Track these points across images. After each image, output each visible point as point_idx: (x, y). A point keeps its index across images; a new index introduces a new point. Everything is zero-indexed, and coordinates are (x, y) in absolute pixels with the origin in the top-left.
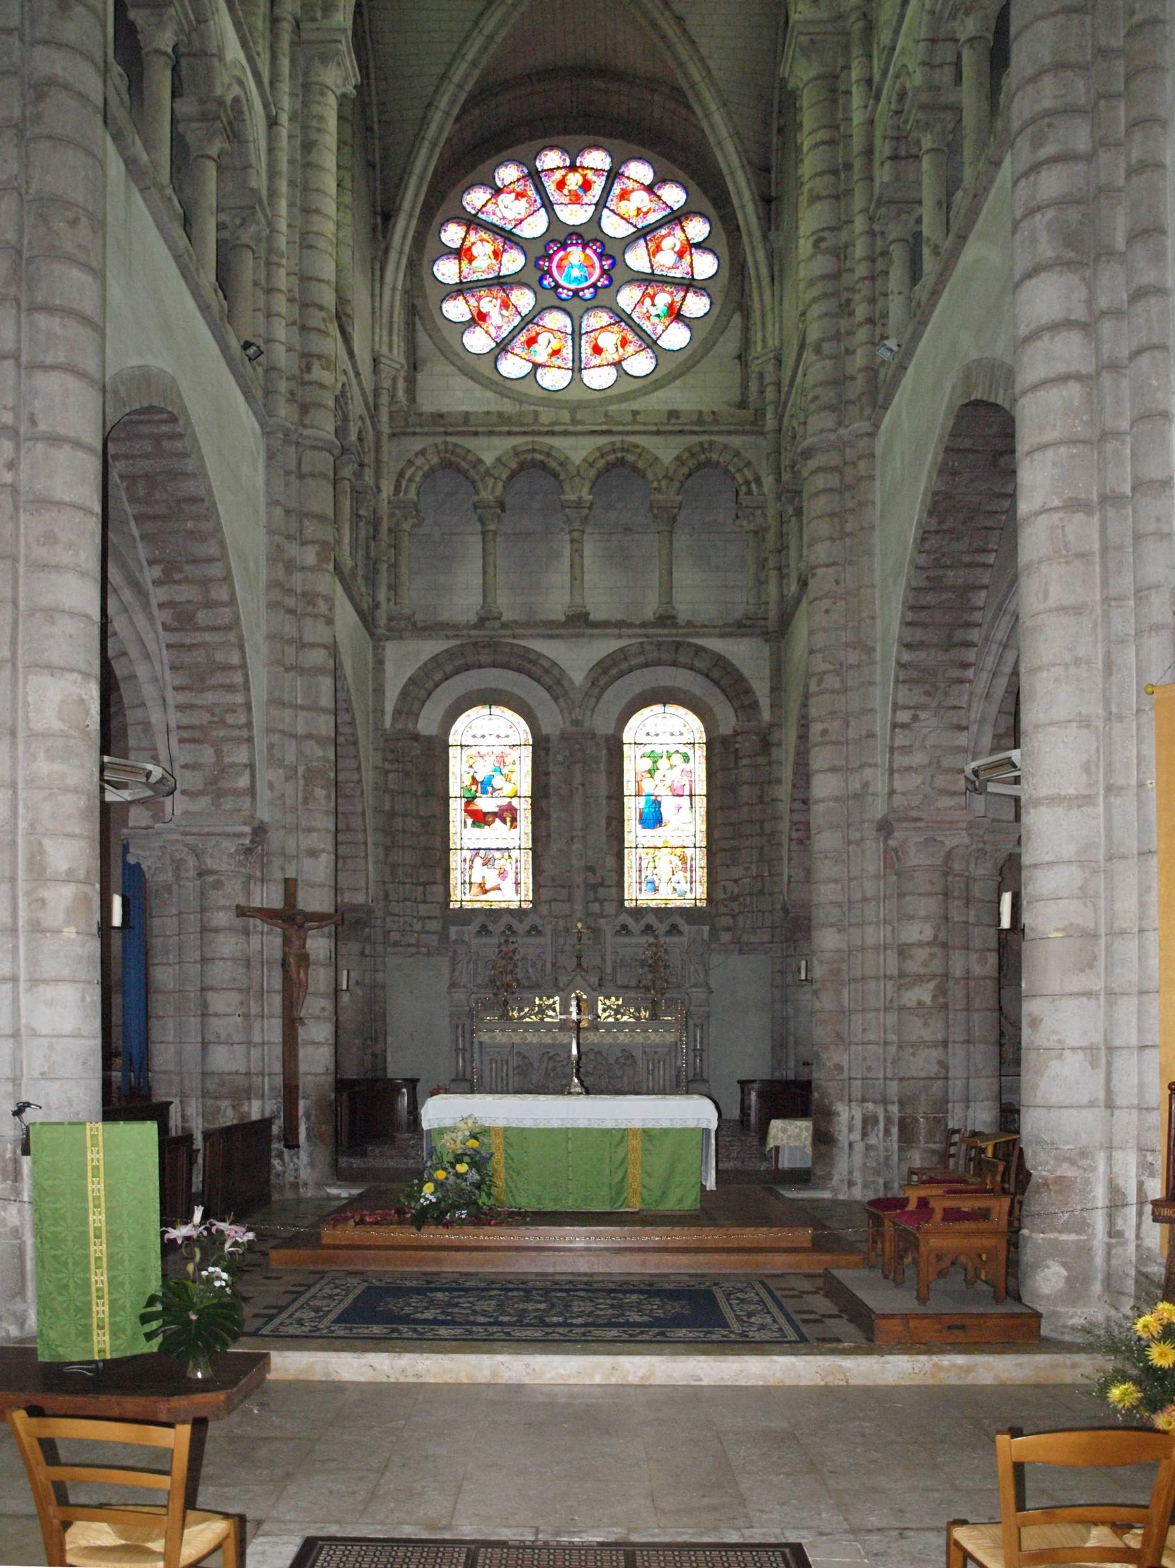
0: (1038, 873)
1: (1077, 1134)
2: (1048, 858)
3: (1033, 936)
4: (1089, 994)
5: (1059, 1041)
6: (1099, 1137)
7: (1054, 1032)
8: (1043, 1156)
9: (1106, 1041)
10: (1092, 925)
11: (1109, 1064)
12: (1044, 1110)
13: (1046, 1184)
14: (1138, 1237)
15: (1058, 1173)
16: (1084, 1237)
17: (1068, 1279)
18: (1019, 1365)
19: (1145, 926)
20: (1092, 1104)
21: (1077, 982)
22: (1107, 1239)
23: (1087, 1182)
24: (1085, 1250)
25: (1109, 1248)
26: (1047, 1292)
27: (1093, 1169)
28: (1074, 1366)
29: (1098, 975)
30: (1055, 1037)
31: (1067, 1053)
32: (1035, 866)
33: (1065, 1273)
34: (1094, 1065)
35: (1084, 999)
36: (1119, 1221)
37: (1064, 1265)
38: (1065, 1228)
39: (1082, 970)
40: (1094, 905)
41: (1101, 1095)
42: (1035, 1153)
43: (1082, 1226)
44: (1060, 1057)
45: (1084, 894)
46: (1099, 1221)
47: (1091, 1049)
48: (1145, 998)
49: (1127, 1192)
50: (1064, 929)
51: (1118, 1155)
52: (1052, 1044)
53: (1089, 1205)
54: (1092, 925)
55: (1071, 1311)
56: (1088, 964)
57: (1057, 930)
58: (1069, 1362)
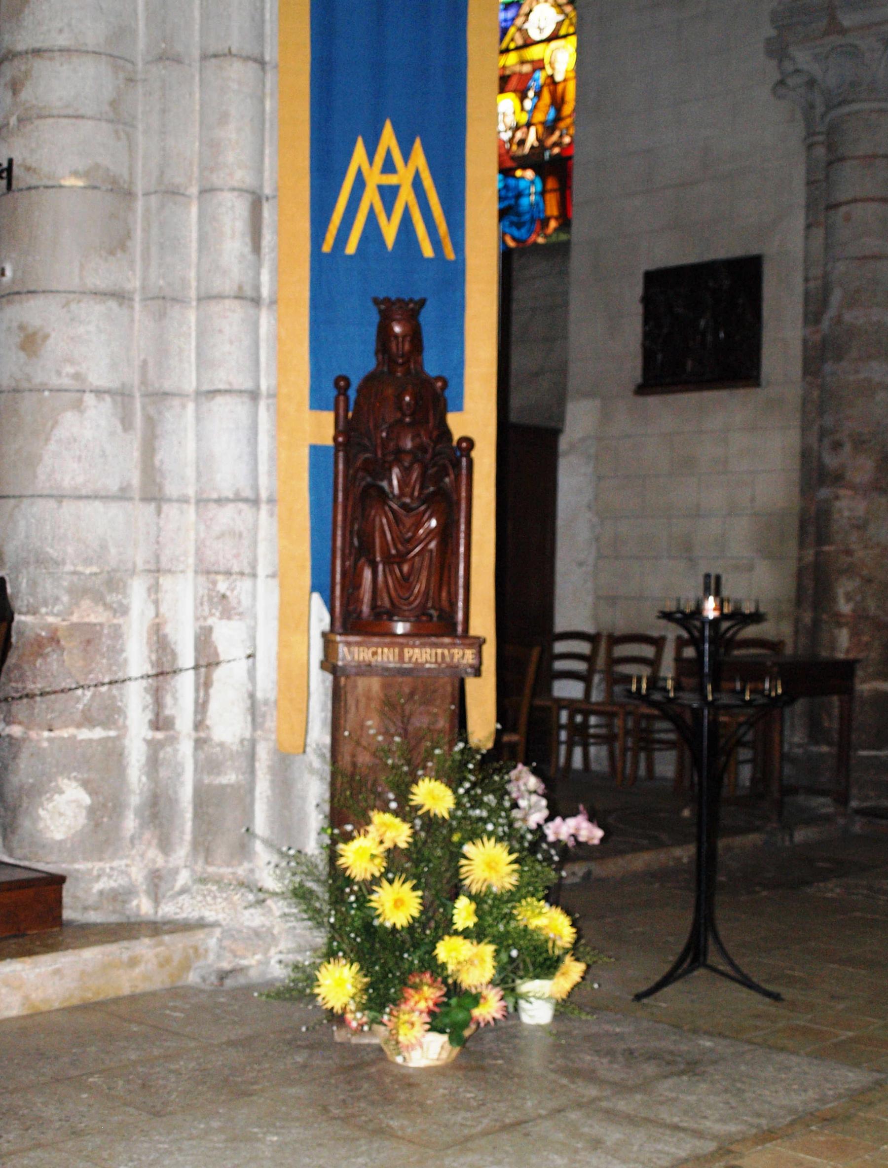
0: (39, 66)
1: (104, 547)
2: (62, 41)
3: (33, 181)
4: (121, 296)
5: (77, 376)
6: (140, 557)
7: (70, 360)
8: (48, 587)
9: (144, 382)
10: (126, 177)
11: (151, 423)
12: (52, 504)
13: (54, 639)
14: (199, 725)
15: (75, 618)
16: (112, 733)
17: (91, 811)
18: (57, 972)
19: (217, 179)
20: (123, 495)
21: (101, 274)
22: (150, 734)
23: (117, 633)
24: (113, 754)
25: (154, 747)
26: (59, 836)
27: (124, 610)
28: (133, 962)
29: (132, 263)
30: (69, 369)
31: (89, 399)
32: (37, 52)
33: (87, 800)
34: (126, 423)
35: (113, 304)
36: (168, 700)
37: (85, 784)
38: (88, 720)
39: (112, 253)
40: (129, 137)
41: (136, 480)
42: (33, 584)
43: (110, 714)
44: (78, 406)
45: (118, 116)
46: (135, 701)
47: (121, 396)
48: (215, 308)
49: (179, 649)
50: (86, 174)
51: (166, 582)
52: (66, 382)
53: (120, 675)
54: (126, 177)
55: (96, 866)
56: (118, 244)
57: (75, 174)
58: (125, 956)
